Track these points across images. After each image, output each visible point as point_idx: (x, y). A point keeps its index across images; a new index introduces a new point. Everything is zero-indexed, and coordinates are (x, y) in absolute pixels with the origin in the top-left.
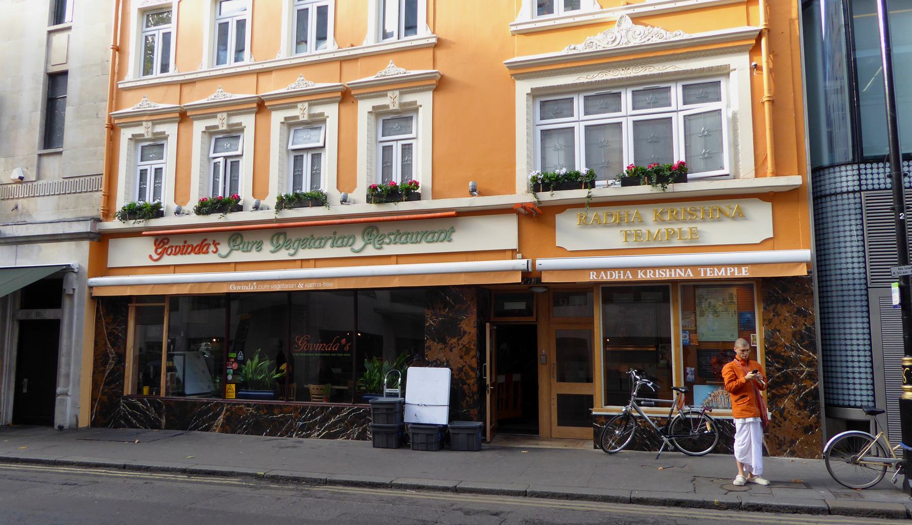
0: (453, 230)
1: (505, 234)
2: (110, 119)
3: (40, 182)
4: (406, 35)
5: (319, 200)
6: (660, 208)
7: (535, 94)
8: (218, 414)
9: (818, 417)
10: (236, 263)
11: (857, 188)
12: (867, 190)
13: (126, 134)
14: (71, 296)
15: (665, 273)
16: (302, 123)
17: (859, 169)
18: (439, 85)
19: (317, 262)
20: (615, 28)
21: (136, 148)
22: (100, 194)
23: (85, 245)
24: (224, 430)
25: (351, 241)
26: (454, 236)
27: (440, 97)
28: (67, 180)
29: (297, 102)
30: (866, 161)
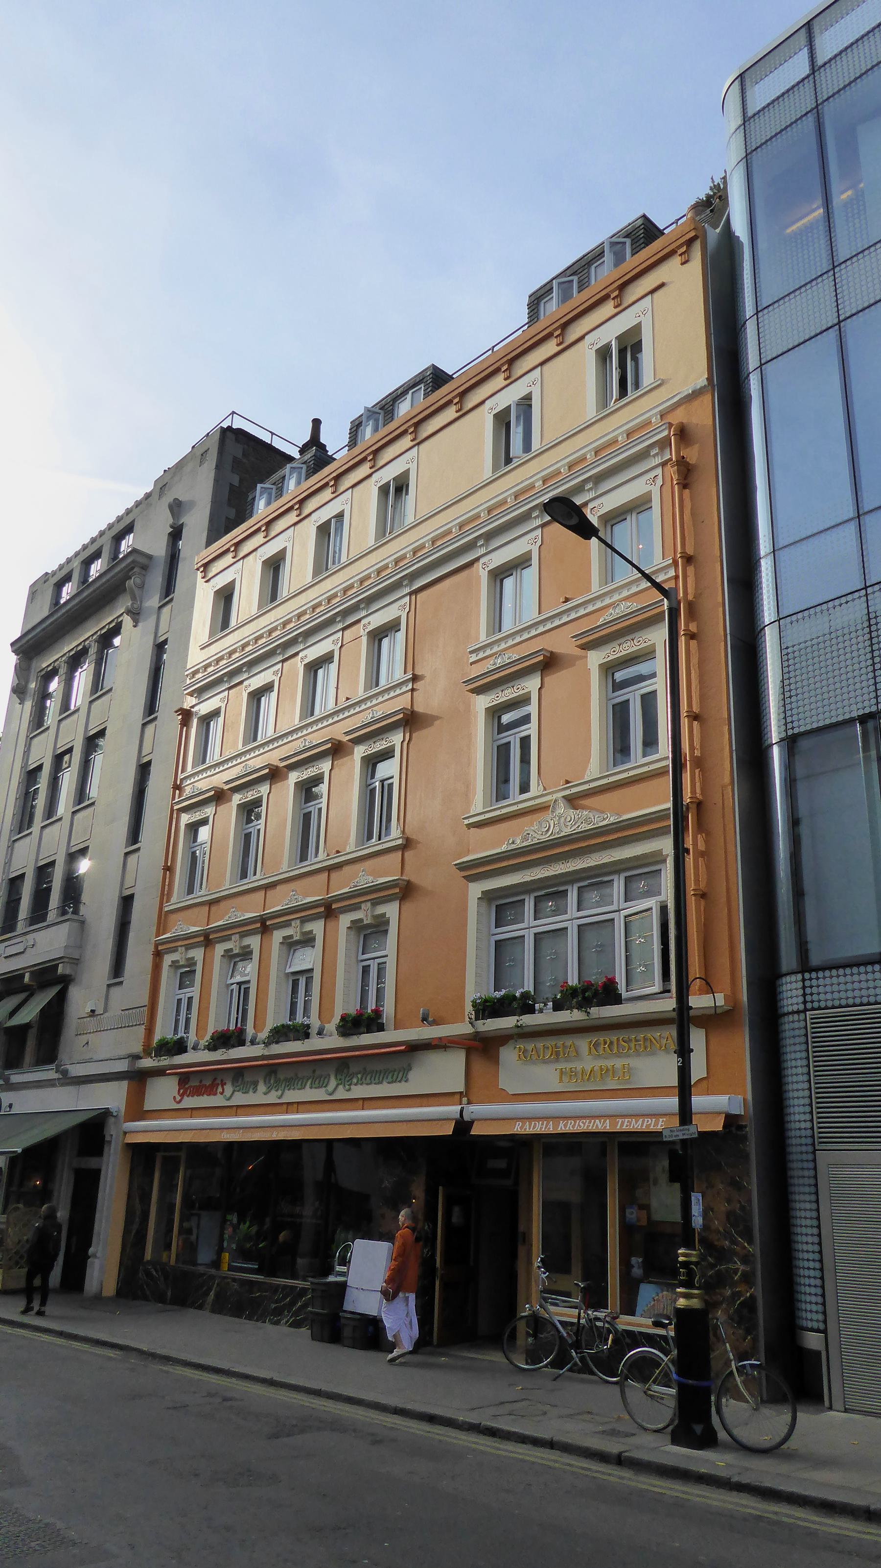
0: (410, 1068)
1: (446, 1072)
2: (156, 946)
3: (106, 1015)
4: (644, 756)
5: (303, 1033)
6: (594, 1038)
7: (488, 897)
8: (210, 1289)
9: (755, 1340)
10: (238, 1106)
11: (801, 1007)
12: (813, 1009)
13: (168, 959)
14: (110, 1142)
15: (584, 1124)
16: (298, 942)
17: (803, 980)
18: (405, 891)
19: (298, 1106)
20: (548, 815)
21: (359, 936)
22: (143, 1027)
23: (125, 1084)
24: (213, 1311)
25: (326, 1080)
26: (411, 1075)
27: (408, 906)
28: (127, 1012)
29: (361, 902)
30: (810, 971)
